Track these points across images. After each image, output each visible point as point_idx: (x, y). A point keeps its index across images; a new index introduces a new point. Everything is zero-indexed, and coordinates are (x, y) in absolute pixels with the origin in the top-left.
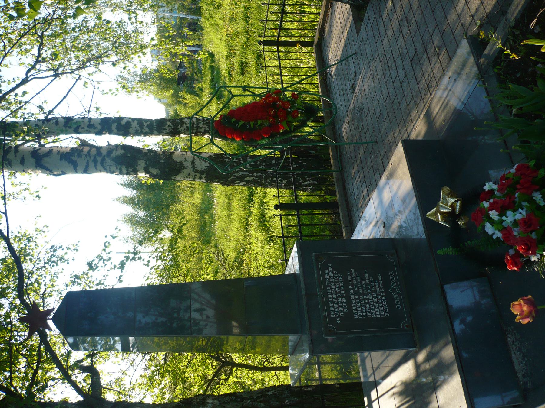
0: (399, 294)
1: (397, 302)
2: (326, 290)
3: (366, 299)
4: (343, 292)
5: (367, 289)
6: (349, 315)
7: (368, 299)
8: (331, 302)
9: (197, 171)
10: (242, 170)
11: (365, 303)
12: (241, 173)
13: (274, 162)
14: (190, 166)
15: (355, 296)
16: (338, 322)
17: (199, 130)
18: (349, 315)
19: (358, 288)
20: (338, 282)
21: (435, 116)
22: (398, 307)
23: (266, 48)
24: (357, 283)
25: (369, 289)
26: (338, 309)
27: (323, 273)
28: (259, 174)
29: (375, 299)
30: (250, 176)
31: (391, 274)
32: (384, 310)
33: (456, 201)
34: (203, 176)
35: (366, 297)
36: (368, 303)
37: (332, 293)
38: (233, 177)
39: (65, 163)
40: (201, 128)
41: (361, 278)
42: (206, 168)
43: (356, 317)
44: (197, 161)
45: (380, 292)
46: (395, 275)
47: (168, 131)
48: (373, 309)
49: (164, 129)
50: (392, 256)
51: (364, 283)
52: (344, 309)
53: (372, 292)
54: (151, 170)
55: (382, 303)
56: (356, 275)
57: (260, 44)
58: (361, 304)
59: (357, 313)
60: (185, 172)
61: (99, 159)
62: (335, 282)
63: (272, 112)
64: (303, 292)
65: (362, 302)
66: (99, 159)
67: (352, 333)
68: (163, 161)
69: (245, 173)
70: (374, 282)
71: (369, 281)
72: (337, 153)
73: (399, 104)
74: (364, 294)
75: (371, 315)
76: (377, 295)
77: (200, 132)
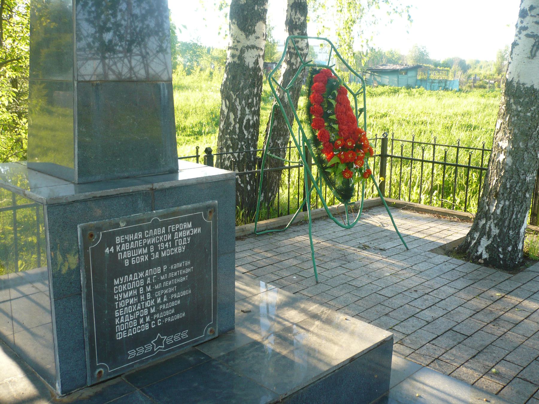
0: (153, 351)
1: (141, 350)
2: (160, 225)
3: (146, 297)
4: (157, 256)
5: (162, 297)
6: (119, 269)
7: (146, 300)
8: (140, 236)
9: (242, 52)
10: (243, 110)
11: (139, 295)
12: (239, 108)
13: (252, 149)
14: (249, 43)
15: (151, 276)
16: (107, 250)
17: (294, 56)
18: (119, 269)
19: (164, 280)
20: (173, 246)
21: (417, 381)
22: (132, 353)
24: (171, 279)
25: (162, 299)
26: (129, 249)
28: (237, 131)
29: (146, 312)
30: (235, 120)
31: (184, 334)
32: (127, 330)
34: (236, 59)
35: (149, 296)
36: (139, 301)
37: (155, 236)
38: (234, 97)
40: (296, 59)
41: (178, 284)
42: (247, 64)
43: (116, 282)
44: (255, 52)
45: (156, 319)
46: (182, 341)
47: (293, 17)
48: (129, 310)
49: (296, 13)
50: (211, 331)
51: (171, 290)
52: (130, 259)
53: (157, 305)
55: (139, 324)
56: (184, 275)
57: (383, 135)
58: (138, 289)
59: (124, 283)
60: (242, 36)
62: (173, 240)
63: (349, 144)
64: (157, 186)
65: (141, 290)
67: (88, 278)
68: (256, 8)
69: (239, 112)
70: (171, 308)
71: (174, 299)
72: (273, 229)
73: (386, 315)
74: (153, 292)
75: (119, 308)
76: (151, 315)
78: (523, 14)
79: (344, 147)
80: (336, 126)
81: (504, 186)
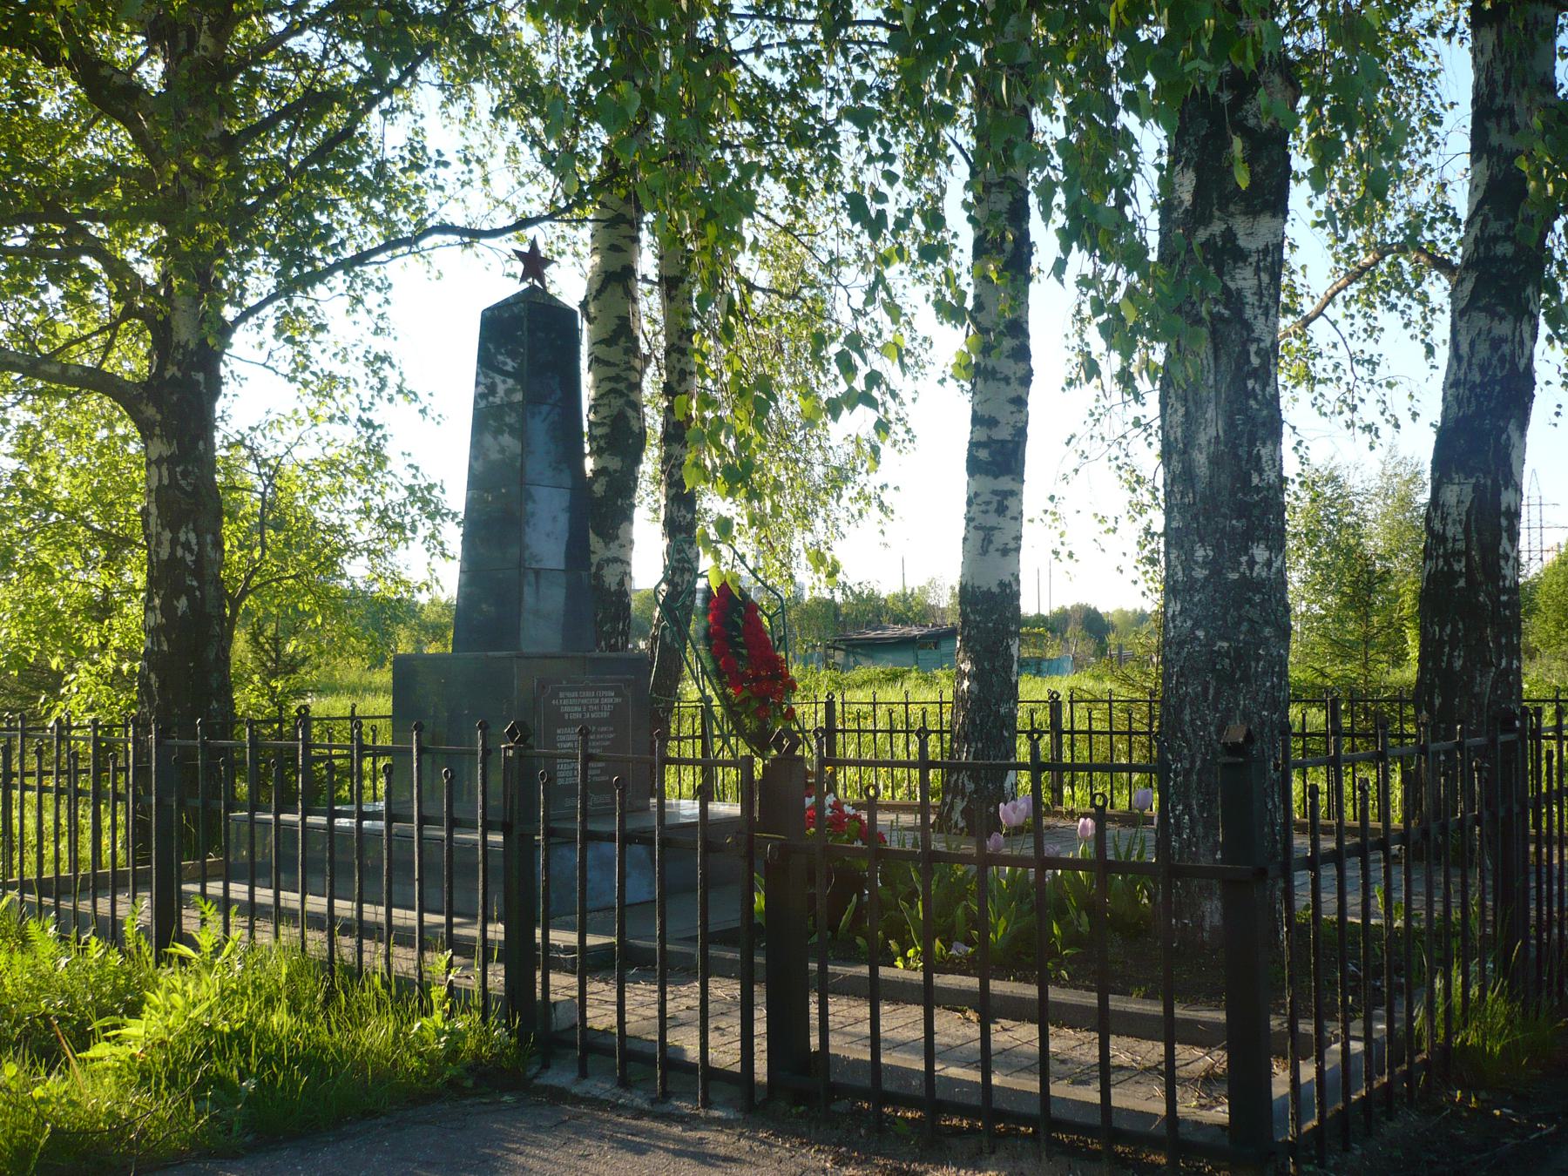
2: (591, 689)
14: (609, 554)
23: (822, 707)
27: (611, 688)
33: (536, 1076)
39: (613, 324)
40: (682, 575)
54: (603, 480)
61: (622, 386)
66: (622, 386)
77: (674, 574)
78: (970, 503)
79: (757, 678)
80: (744, 652)
81: (973, 721)
